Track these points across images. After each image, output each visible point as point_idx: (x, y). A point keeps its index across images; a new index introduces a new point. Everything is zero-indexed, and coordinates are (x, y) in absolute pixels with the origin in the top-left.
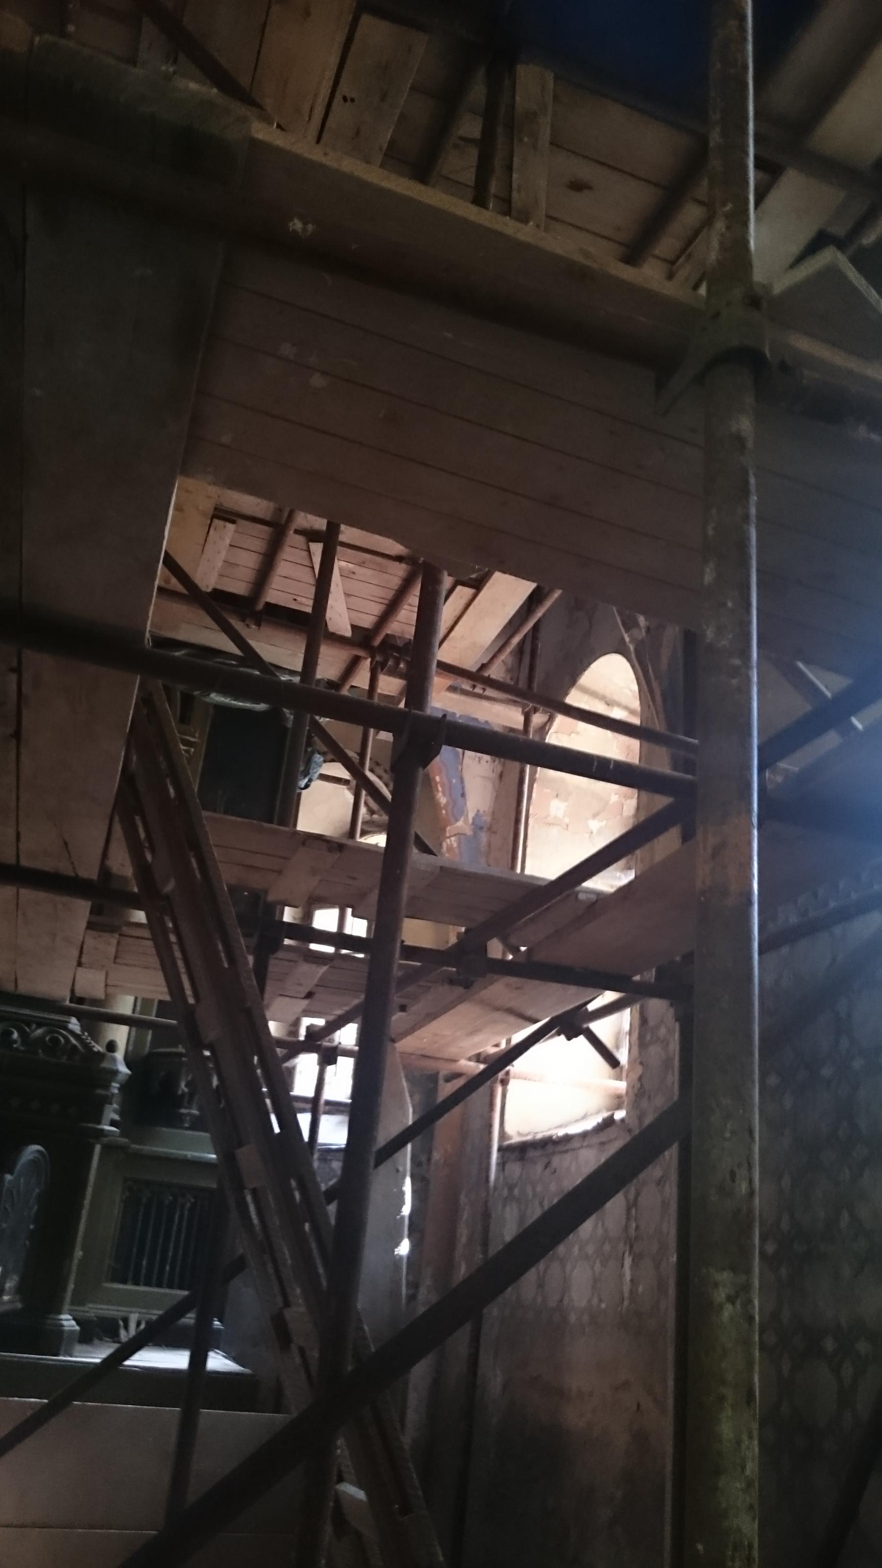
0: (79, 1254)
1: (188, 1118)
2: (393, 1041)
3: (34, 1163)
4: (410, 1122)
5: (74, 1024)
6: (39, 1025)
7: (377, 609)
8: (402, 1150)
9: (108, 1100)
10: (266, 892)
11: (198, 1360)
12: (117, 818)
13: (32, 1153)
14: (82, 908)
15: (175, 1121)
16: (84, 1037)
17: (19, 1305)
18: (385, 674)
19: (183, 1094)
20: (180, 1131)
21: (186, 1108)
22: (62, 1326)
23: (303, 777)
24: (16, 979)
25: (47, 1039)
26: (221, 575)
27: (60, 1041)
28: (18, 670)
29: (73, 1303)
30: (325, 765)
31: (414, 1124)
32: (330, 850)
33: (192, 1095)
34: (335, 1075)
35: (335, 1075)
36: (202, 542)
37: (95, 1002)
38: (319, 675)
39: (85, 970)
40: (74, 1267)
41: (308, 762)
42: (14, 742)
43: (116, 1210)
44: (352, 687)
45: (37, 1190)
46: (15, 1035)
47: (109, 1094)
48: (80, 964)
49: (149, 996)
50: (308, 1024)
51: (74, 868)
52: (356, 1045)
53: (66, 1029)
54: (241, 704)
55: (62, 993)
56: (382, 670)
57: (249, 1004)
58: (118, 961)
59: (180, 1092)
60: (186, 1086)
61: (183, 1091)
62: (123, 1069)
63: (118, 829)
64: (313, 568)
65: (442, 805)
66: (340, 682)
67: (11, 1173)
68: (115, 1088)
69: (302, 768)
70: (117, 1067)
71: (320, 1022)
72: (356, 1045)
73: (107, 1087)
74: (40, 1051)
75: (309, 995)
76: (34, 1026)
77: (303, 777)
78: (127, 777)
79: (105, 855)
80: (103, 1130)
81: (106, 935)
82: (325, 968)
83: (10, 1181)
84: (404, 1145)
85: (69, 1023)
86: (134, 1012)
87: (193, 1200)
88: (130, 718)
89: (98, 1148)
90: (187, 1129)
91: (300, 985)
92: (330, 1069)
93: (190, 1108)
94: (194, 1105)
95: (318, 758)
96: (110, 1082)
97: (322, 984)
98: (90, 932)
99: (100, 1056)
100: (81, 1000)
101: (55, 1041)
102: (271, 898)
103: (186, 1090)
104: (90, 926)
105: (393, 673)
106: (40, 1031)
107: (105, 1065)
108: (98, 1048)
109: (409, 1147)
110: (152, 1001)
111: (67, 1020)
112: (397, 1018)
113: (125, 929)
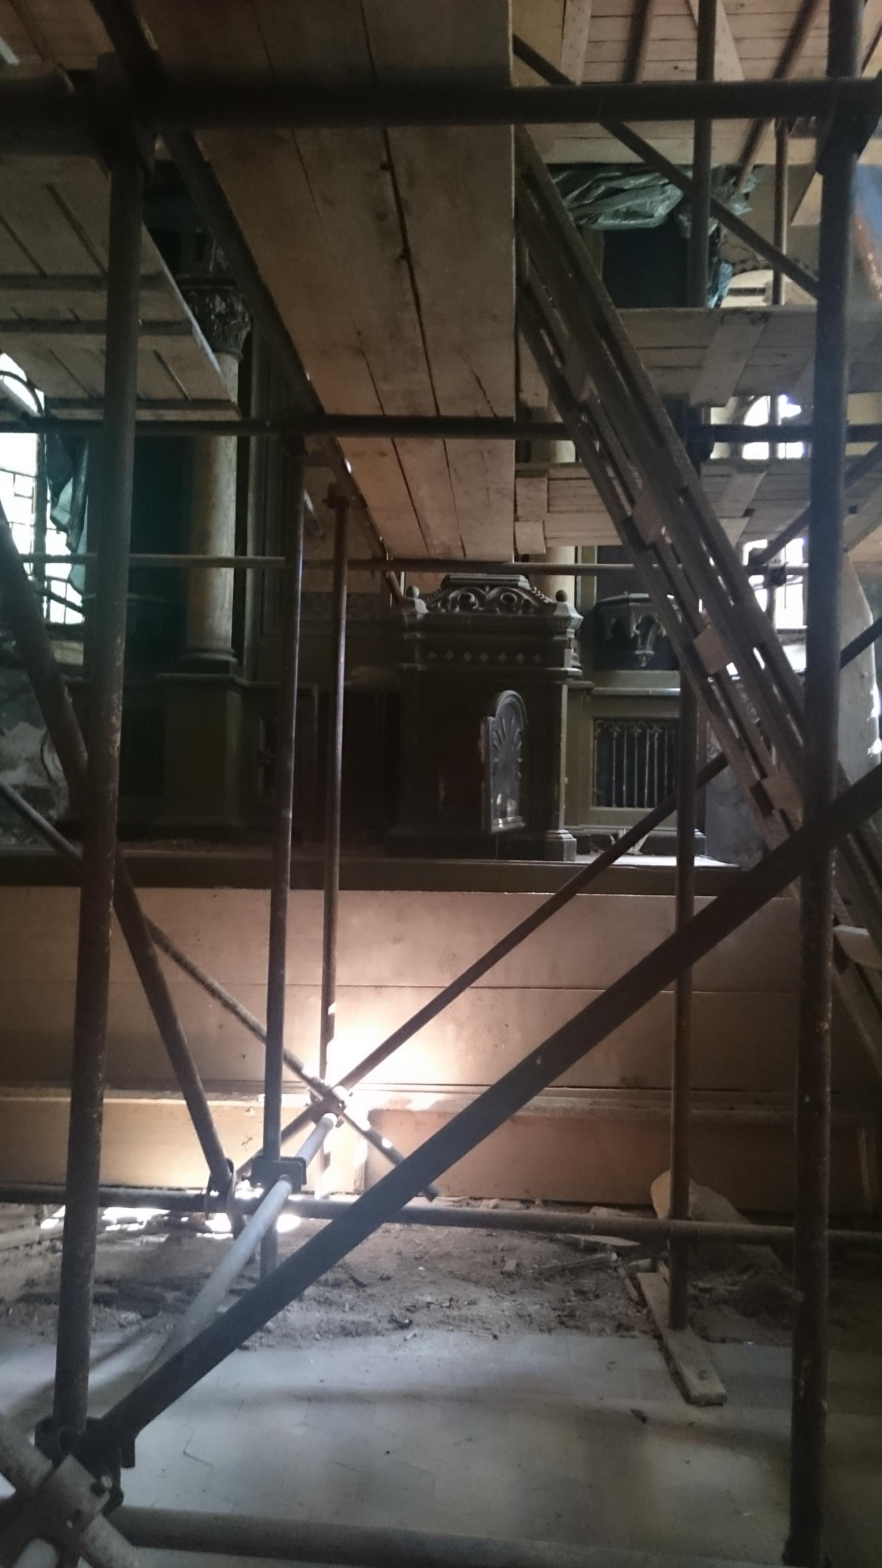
0: (564, 780)
1: (644, 658)
2: (846, 551)
3: (511, 705)
4: (872, 622)
5: (523, 582)
6: (492, 587)
7: (774, 48)
8: (867, 649)
9: (566, 644)
10: (687, 395)
11: (685, 861)
12: (522, 338)
13: (507, 697)
14: (508, 447)
15: (632, 663)
16: (534, 592)
17: (522, 825)
18: (794, 136)
19: (636, 636)
20: (637, 672)
21: (640, 649)
22: (561, 838)
23: (712, 296)
24: (448, 467)
25: (501, 598)
26: (587, 62)
27: (513, 598)
28: (388, 167)
29: (566, 824)
30: (734, 279)
31: (876, 624)
32: (753, 322)
33: (644, 637)
34: (785, 607)
35: (785, 607)
36: (560, 22)
37: (539, 557)
38: (714, 164)
39: (523, 524)
40: (563, 791)
41: (716, 276)
42: (404, 263)
43: (592, 743)
44: (756, 167)
45: (518, 730)
46: (473, 598)
47: (567, 639)
48: (516, 519)
49: (589, 543)
50: (750, 549)
51: (491, 407)
52: (804, 562)
53: (516, 586)
54: (632, 222)
55: (506, 553)
56: (790, 130)
57: (685, 483)
58: (552, 509)
59: (632, 635)
60: (637, 628)
61: (635, 633)
62: (575, 615)
63: (526, 351)
64: (691, 15)
65: (879, 288)
66: (741, 165)
67: (494, 716)
68: (571, 633)
69: (709, 285)
70: (568, 613)
71: (762, 544)
72: (804, 562)
73: (564, 633)
74: (498, 609)
75: (748, 513)
76: (488, 589)
77: (712, 296)
78: (525, 288)
79: (518, 389)
80: (566, 672)
81: (535, 480)
82: (761, 477)
83: (493, 722)
84: (868, 644)
85: (519, 581)
86: (576, 561)
87: (660, 731)
88: (513, 197)
89: (565, 689)
90: (645, 668)
91: (737, 501)
92: (779, 591)
93: (644, 649)
94: (648, 646)
95: (726, 268)
96: (566, 628)
97: (761, 496)
98: (520, 480)
99: (553, 607)
100: (526, 558)
101: (509, 599)
102: (693, 401)
103: (638, 632)
104: (518, 474)
105: (802, 133)
106: (494, 592)
107: (558, 613)
108: (548, 600)
109: (873, 645)
110: (592, 548)
111: (517, 578)
112: (848, 520)
113: (553, 472)
